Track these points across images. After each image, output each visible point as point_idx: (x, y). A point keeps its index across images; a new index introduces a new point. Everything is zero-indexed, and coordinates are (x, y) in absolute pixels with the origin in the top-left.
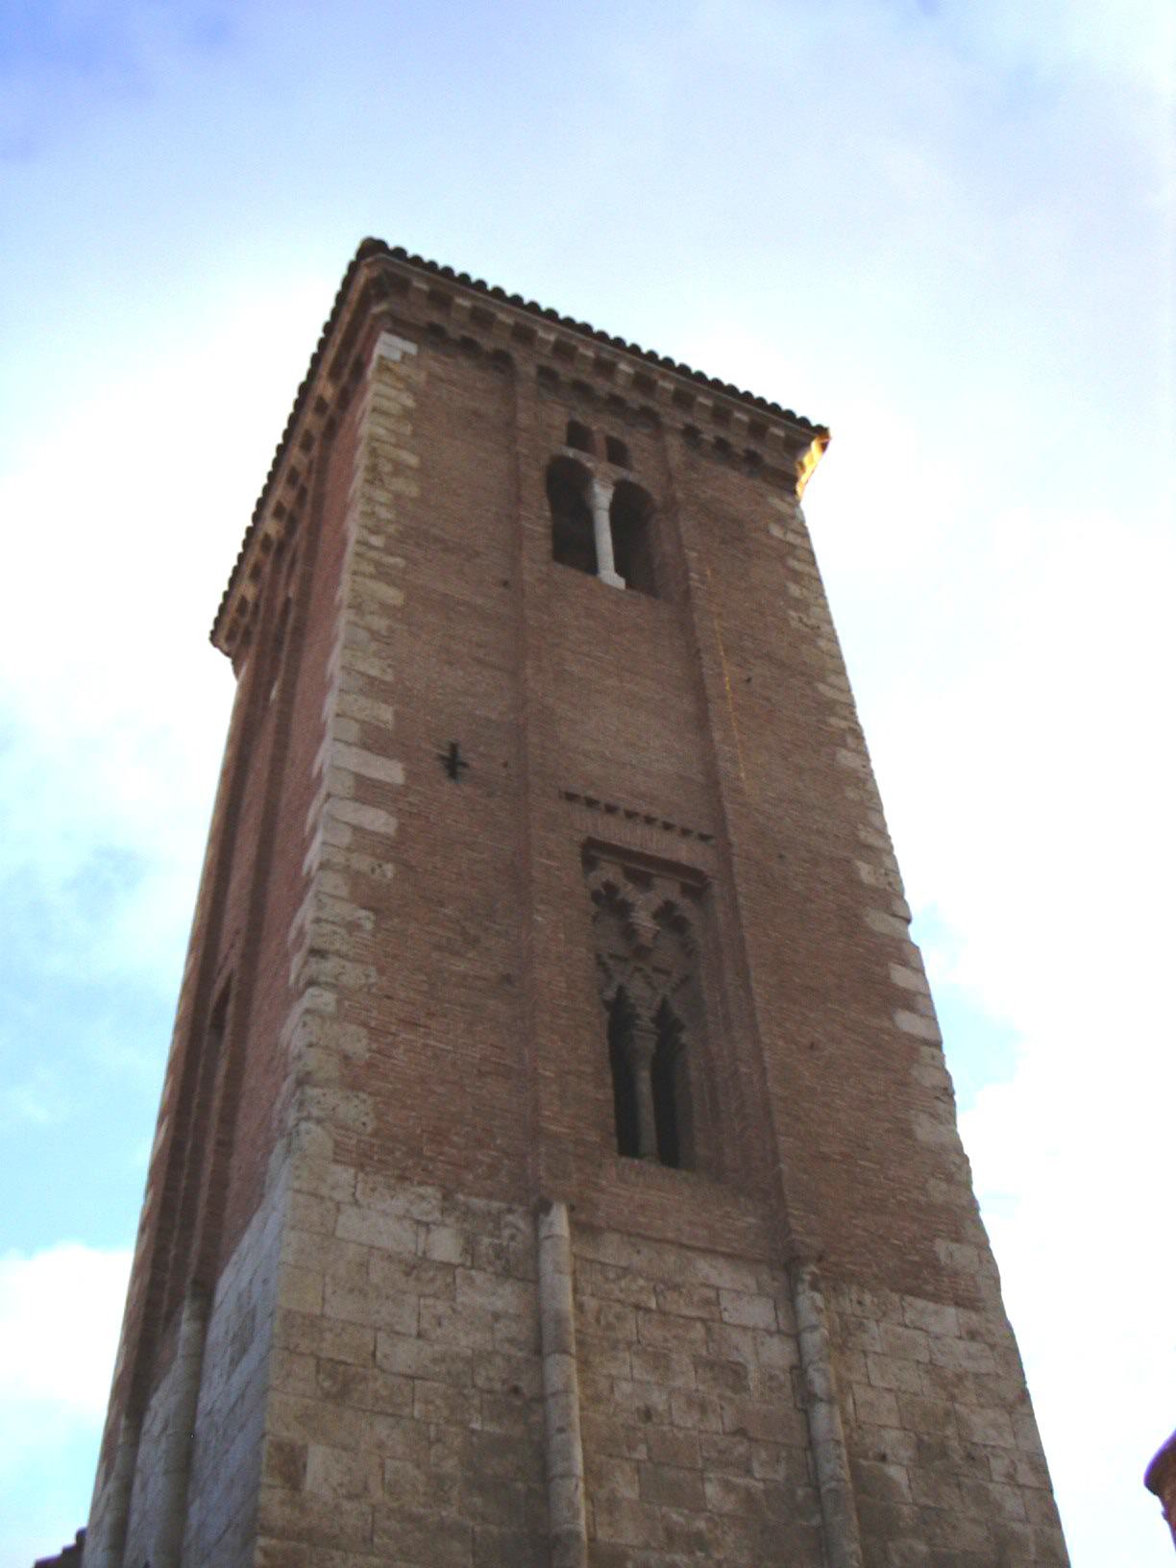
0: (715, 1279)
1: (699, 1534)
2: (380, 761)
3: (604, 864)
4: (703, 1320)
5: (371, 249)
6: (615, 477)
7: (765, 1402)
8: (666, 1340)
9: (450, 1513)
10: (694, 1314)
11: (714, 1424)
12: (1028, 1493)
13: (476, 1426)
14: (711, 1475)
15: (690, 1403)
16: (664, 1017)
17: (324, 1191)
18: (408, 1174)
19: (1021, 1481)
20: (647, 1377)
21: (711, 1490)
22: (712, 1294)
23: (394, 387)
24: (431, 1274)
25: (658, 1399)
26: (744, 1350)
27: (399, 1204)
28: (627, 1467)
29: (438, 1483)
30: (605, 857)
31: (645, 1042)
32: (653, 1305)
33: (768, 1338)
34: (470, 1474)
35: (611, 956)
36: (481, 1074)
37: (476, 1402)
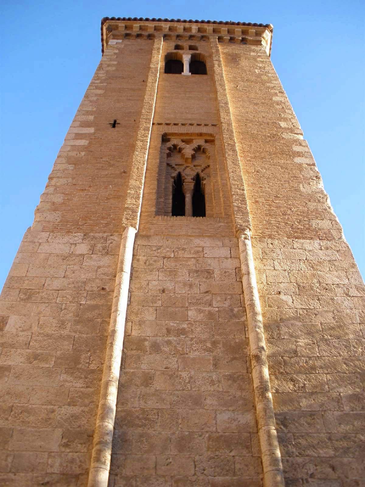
0: (202, 244)
1: (184, 329)
2: (89, 129)
3: (173, 140)
4: (194, 258)
5: (106, 20)
6: (191, 53)
7: (222, 280)
8: (176, 266)
9: (65, 332)
10: (191, 256)
11: (196, 290)
12: (356, 299)
13: (83, 302)
14: (191, 308)
15: (185, 285)
16: (198, 180)
17: (36, 240)
18: (71, 231)
19: (352, 295)
20: (165, 279)
21: (191, 313)
22: (201, 249)
23: (112, 50)
24: (74, 258)
25: (169, 285)
26: (214, 265)
27: (66, 239)
28: (151, 309)
29: (62, 324)
30: (173, 137)
31: (189, 186)
32: (172, 256)
33: (225, 260)
34: (348, 437)
35: (176, 165)
36: (108, 199)
37: (85, 295)
